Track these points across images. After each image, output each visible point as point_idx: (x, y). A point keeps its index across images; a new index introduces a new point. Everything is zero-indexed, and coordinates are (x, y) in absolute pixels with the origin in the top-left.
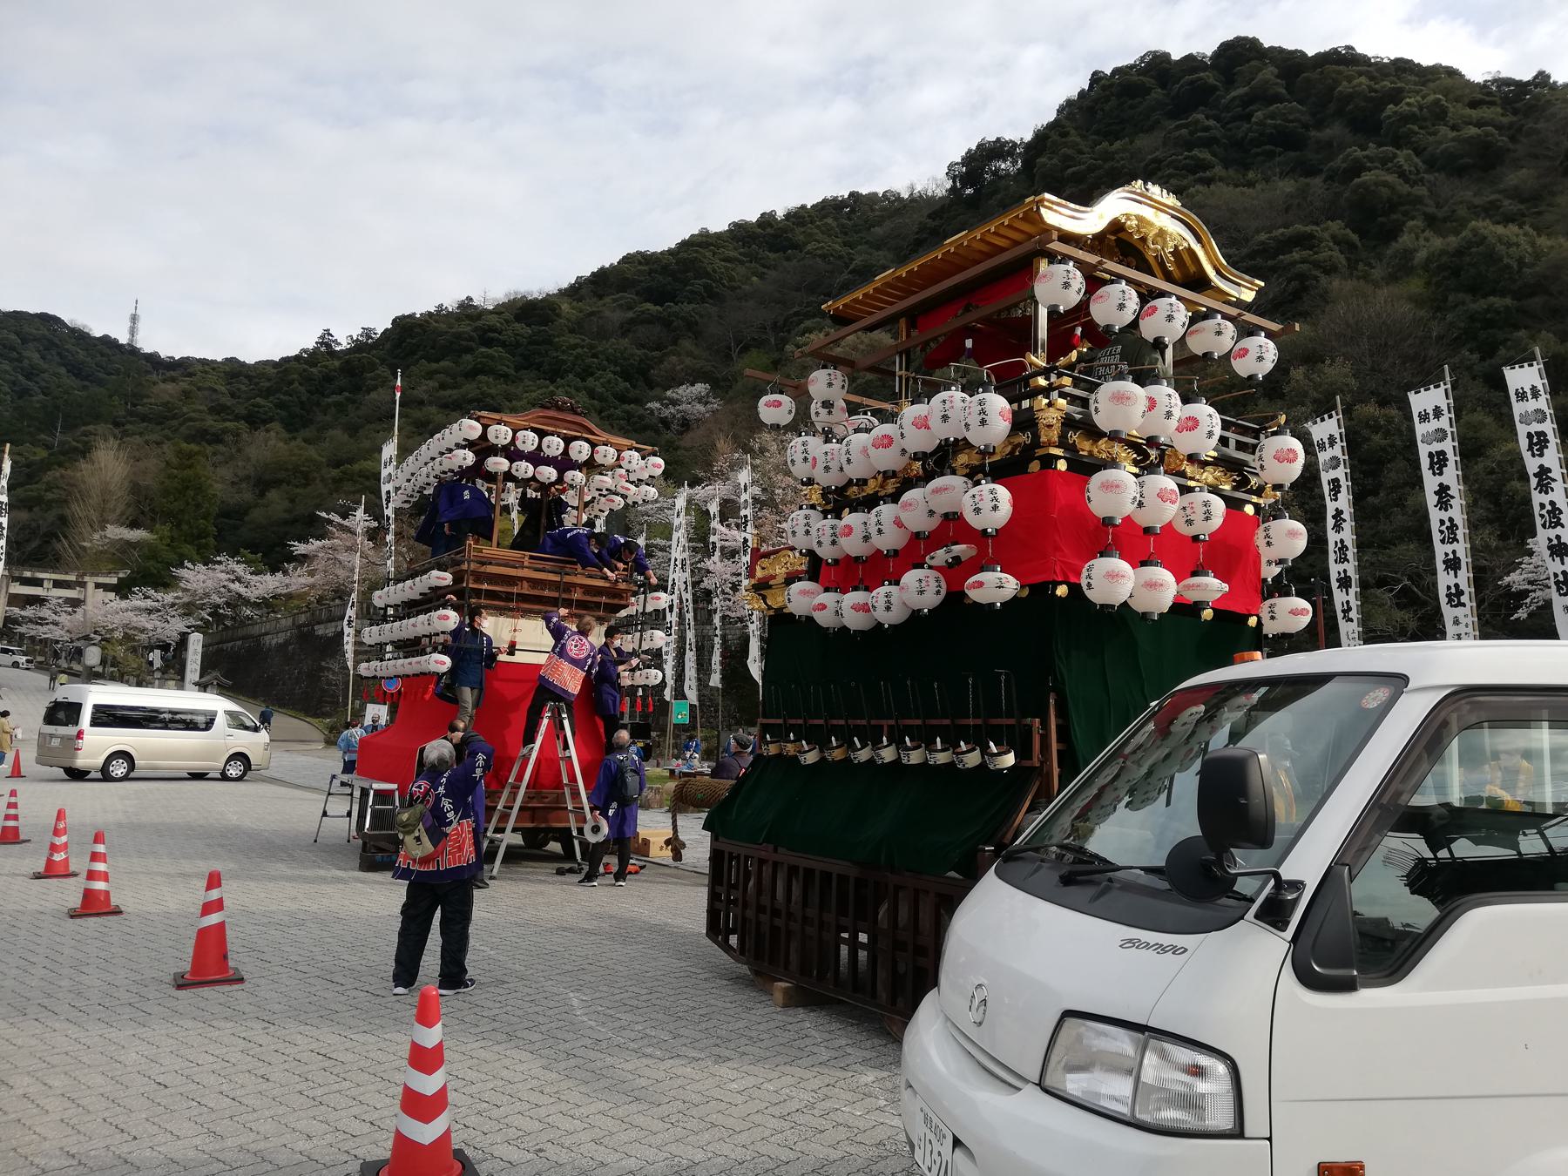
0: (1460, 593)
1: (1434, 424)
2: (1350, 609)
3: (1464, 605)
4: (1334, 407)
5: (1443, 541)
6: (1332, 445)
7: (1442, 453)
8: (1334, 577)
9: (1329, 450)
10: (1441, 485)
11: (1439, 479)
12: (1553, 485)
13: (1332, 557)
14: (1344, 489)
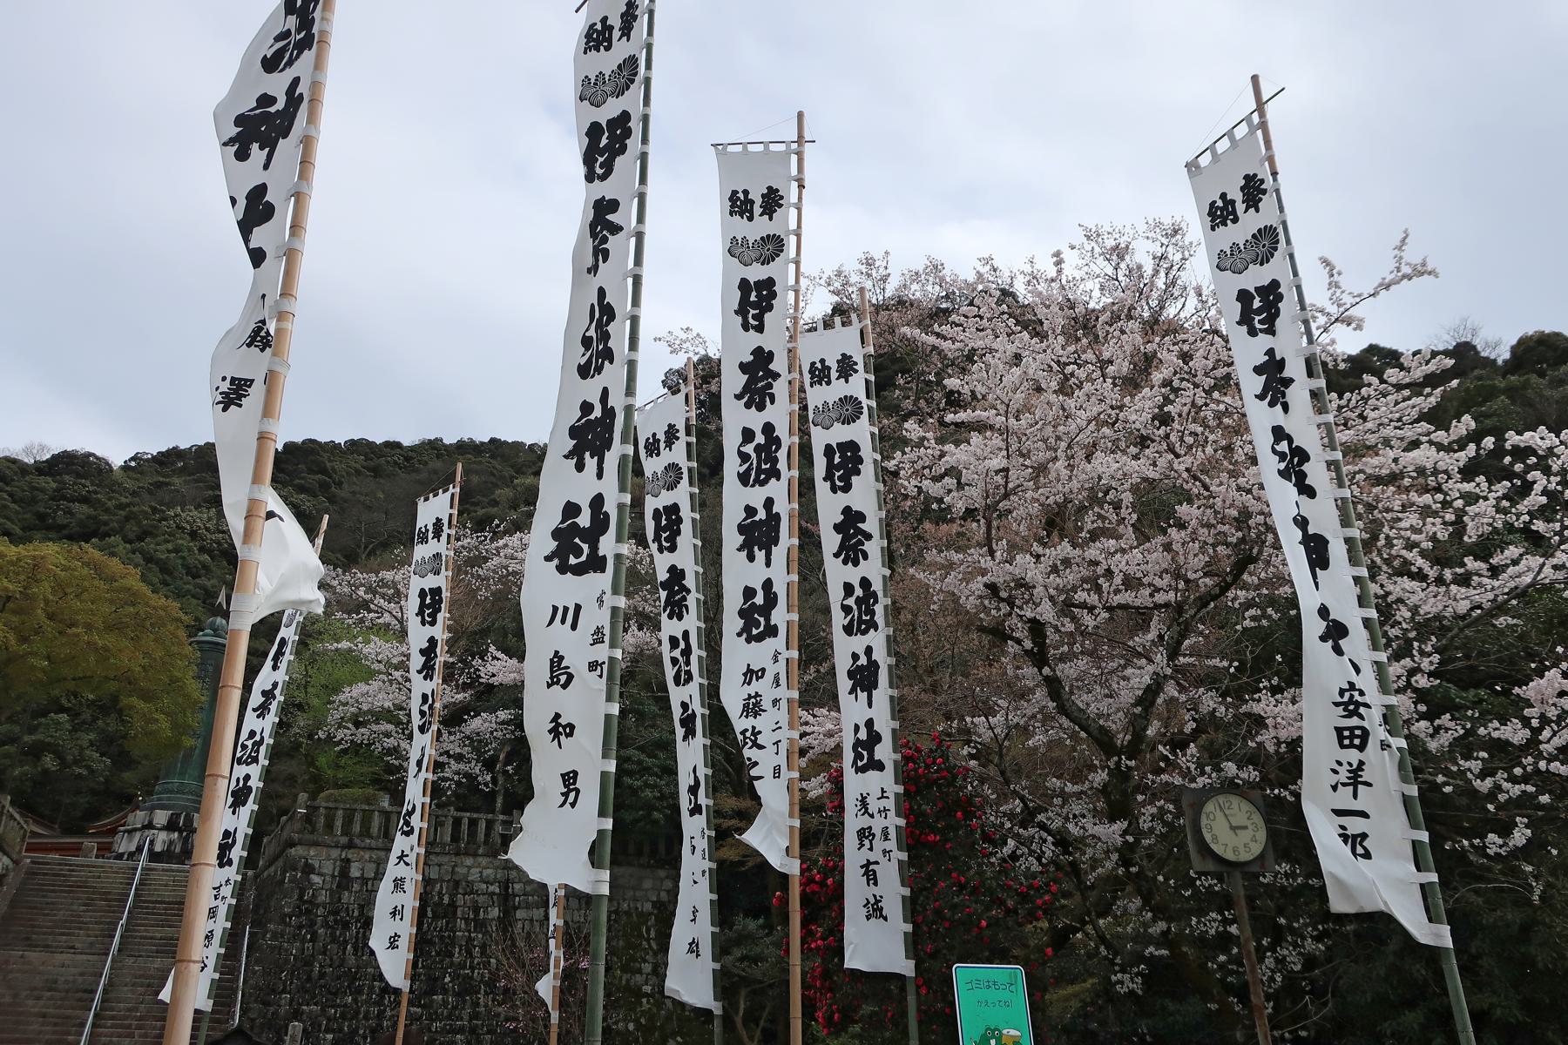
0: (875, 738)
1: (836, 390)
2: (875, 738)
3: (880, 766)
4: (450, 479)
5: (848, 630)
6: (669, 444)
7: (852, 446)
8: (842, 664)
9: (432, 542)
10: (847, 511)
11: (842, 500)
12: (868, 546)
13: (838, 619)
14: (686, 528)
